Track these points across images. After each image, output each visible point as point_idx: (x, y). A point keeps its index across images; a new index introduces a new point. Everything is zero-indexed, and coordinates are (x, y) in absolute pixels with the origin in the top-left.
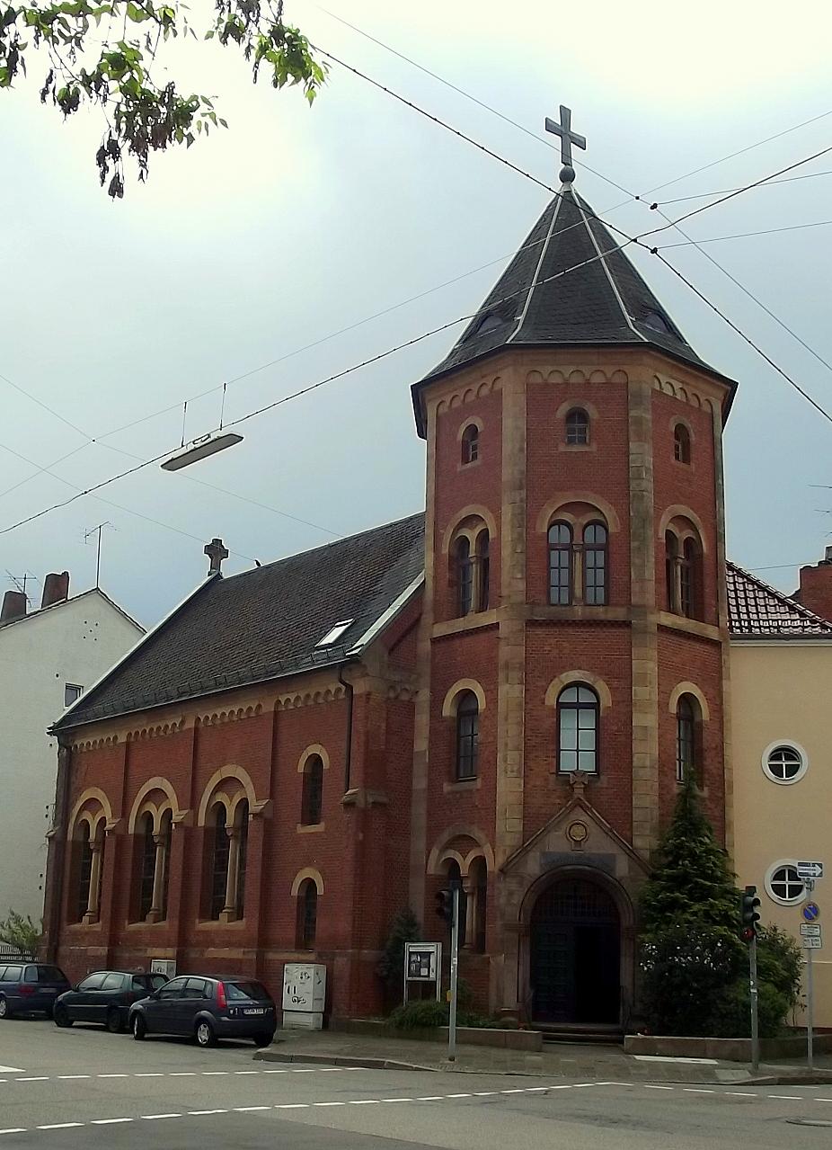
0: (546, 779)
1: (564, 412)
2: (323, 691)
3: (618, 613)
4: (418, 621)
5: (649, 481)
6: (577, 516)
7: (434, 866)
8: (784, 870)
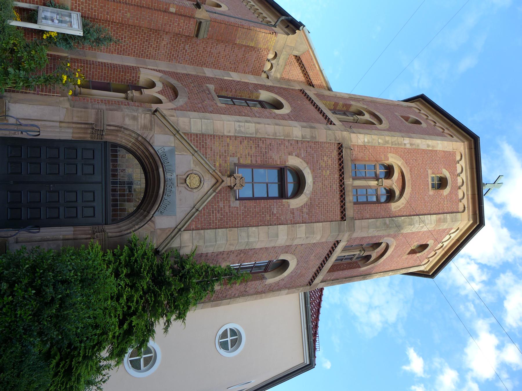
0: (233, 155)
3: (350, 212)
6: (396, 182)
8: (151, 353)
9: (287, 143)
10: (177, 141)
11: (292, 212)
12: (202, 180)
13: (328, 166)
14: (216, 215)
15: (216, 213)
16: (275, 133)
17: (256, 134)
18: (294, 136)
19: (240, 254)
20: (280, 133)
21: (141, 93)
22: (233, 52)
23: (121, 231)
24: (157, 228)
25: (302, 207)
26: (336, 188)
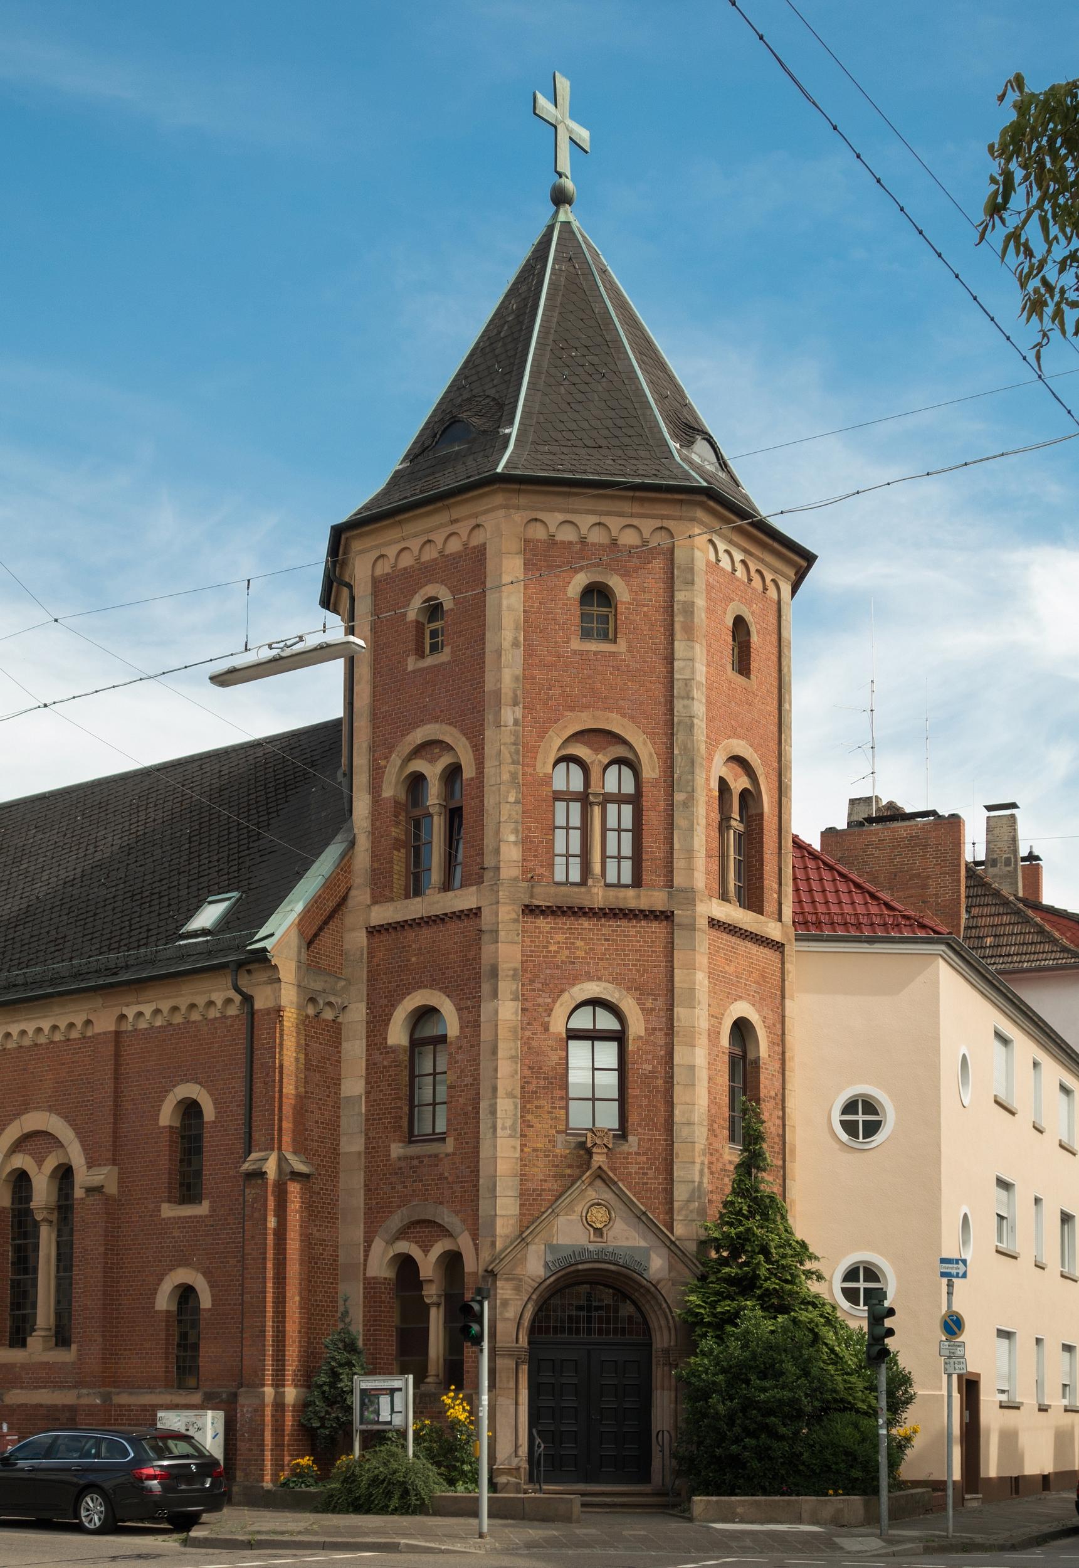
0: (552, 1141)
1: (579, 589)
2: (201, 1001)
3: (653, 898)
4: (344, 899)
5: (700, 702)
6: (596, 751)
7: (380, 1265)
9: (528, 1033)
10: (536, 1240)
11: (651, 1031)
12: (596, 1201)
13: (566, 943)
14: (651, 1178)
15: (648, 1179)
16: (512, 1057)
17: (515, 1097)
18: (513, 1017)
19: (714, 1131)
20: (511, 1049)
21: (431, 1281)
22: (312, 1093)
23: (669, 1327)
24: (667, 1277)
25: (642, 1010)
26: (610, 926)
